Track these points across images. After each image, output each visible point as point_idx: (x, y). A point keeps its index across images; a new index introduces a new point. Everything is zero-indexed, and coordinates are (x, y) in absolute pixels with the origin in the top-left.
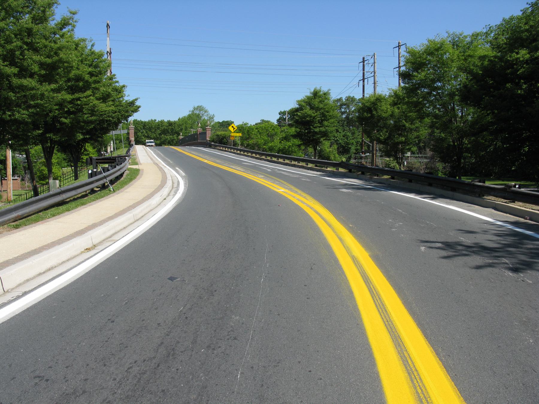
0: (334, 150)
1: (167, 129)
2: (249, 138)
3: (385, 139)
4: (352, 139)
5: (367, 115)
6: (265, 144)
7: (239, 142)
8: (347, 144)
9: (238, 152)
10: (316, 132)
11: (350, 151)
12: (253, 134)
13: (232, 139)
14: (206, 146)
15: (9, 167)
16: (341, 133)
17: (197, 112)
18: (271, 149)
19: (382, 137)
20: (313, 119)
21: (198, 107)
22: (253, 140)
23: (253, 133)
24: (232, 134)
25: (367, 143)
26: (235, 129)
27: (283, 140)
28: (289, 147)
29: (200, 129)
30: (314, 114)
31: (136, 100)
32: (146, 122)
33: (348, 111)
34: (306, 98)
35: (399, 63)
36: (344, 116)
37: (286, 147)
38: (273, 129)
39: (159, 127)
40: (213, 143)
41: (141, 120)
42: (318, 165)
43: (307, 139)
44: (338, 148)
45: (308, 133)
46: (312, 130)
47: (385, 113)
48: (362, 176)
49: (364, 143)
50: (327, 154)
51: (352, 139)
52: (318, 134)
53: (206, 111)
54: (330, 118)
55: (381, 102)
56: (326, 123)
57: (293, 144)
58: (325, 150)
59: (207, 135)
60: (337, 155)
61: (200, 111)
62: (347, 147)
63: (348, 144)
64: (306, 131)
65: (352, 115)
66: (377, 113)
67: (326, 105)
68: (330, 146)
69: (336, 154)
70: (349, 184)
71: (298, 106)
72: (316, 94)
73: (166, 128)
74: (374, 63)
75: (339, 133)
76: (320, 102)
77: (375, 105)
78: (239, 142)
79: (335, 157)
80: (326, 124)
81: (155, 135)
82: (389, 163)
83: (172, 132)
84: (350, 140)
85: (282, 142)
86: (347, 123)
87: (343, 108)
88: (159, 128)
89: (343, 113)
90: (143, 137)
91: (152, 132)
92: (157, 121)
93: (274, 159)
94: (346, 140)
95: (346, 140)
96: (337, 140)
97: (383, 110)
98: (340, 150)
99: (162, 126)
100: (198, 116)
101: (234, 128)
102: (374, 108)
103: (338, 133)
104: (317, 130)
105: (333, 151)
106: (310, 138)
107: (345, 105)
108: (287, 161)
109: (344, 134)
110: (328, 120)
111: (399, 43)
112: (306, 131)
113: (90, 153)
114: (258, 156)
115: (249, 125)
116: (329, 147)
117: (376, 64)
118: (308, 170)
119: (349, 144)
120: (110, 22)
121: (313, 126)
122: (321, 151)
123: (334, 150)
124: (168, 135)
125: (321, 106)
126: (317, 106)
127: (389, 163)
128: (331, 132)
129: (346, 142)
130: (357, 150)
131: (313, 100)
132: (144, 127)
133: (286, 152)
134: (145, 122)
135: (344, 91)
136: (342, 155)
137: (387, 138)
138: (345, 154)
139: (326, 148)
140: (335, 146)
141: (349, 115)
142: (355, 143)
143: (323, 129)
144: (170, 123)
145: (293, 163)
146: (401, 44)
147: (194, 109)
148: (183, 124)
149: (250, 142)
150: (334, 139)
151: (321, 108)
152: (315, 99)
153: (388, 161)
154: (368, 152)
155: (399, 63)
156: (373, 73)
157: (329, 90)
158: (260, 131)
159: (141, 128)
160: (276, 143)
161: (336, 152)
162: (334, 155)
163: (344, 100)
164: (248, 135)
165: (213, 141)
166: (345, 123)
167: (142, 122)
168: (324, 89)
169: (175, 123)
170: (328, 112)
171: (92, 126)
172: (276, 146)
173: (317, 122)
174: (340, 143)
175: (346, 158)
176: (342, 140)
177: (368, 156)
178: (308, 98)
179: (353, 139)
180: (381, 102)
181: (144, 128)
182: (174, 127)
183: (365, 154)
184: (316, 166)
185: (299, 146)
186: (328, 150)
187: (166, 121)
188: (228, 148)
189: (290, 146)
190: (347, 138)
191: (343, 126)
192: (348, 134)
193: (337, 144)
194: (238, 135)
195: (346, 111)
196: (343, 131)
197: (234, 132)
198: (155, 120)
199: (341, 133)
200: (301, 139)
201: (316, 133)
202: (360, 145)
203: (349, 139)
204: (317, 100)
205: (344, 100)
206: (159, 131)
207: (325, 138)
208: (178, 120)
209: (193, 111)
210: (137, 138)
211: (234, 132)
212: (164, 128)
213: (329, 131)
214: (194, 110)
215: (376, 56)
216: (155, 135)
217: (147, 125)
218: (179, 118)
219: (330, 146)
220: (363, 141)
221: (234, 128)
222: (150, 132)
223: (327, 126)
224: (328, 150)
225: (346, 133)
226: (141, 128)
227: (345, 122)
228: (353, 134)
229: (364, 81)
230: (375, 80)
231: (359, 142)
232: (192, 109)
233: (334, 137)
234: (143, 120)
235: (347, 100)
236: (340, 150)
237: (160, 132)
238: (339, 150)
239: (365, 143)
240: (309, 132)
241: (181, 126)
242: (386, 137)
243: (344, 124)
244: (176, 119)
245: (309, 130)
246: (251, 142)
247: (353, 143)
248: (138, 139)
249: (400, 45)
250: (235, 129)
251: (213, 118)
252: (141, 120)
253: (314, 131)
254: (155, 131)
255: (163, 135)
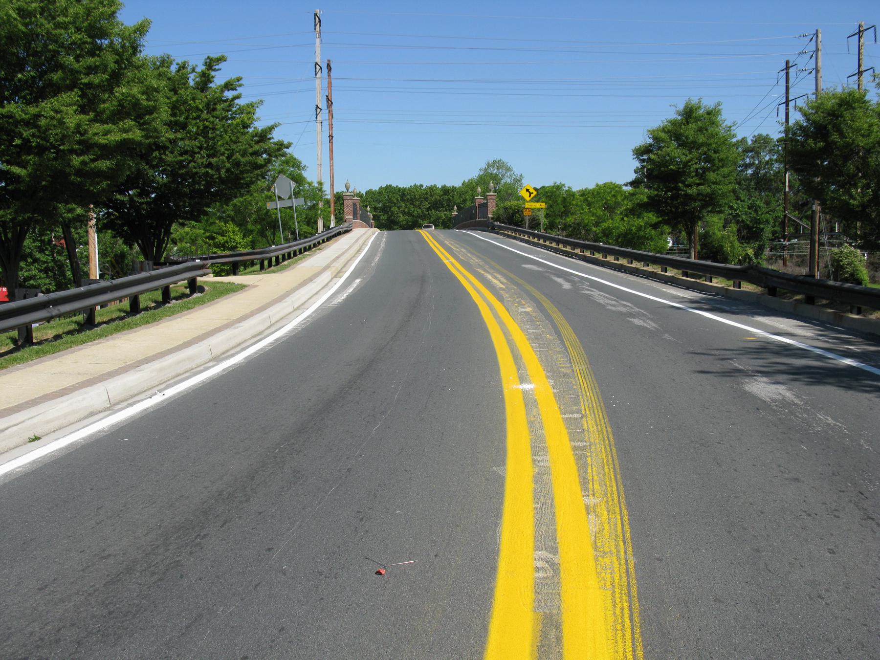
0: (732, 235)
1: (440, 200)
2: (566, 213)
3: (864, 206)
4: (766, 213)
5: (815, 144)
6: (597, 224)
7: (544, 221)
8: (756, 223)
9: (536, 240)
10: (691, 195)
11: (762, 235)
12: (573, 205)
13: (526, 214)
14: (486, 229)
15: (94, 274)
16: (744, 201)
17: (493, 171)
18: (607, 233)
19: (855, 199)
20: (683, 168)
21: (494, 162)
22: (575, 217)
23: (574, 202)
24: (527, 205)
25: (794, 221)
26: (532, 196)
27: (627, 216)
28: (640, 228)
29: (479, 197)
30: (686, 156)
31: (271, 129)
32: (405, 189)
33: (757, 162)
34: (669, 124)
35: (859, 66)
36: (750, 172)
37: (633, 228)
38: (614, 196)
39: (427, 198)
40: (497, 223)
41: (397, 186)
42: (690, 272)
43: (671, 212)
44: (739, 230)
45: (673, 198)
46: (682, 190)
47: (863, 136)
48: (807, 309)
49: (788, 220)
50: (717, 242)
51: (766, 213)
52: (695, 200)
53: (508, 169)
54: (720, 164)
55: (854, 108)
56: (711, 176)
57: (646, 223)
58: (714, 233)
59: (489, 208)
60: (737, 244)
61: (498, 169)
62: (756, 227)
63: (757, 221)
64: (669, 194)
65: (764, 169)
66: (842, 135)
67: (712, 136)
68: (724, 227)
69: (736, 240)
70: (773, 343)
71: (651, 141)
72: (689, 114)
73: (438, 198)
74: (817, 50)
75: (741, 201)
76: (700, 130)
77: (837, 119)
78: (544, 221)
79: (732, 247)
80: (713, 179)
81: (420, 211)
82: (840, 257)
83: (448, 205)
84: (762, 214)
85: (625, 219)
86: (757, 184)
87: (747, 157)
88: (426, 199)
89: (747, 166)
90: (401, 215)
91: (415, 206)
92: (424, 187)
93: (599, 256)
94: (754, 215)
95: (754, 215)
96: (738, 215)
97: (858, 130)
98: (743, 234)
99: (432, 196)
100: (496, 178)
101: (530, 194)
102: (833, 127)
103: (739, 202)
104: (692, 191)
105: (729, 236)
106: (677, 208)
107: (751, 151)
108: (623, 262)
109: (751, 204)
110: (718, 169)
111: (860, 26)
112: (669, 194)
113: (238, 245)
114: (568, 249)
115: (567, 189)
116: (722, 228)
117: (820, 53)
118: (666, 283)
119: (760, 223)
120: (320, 12)
121: (683, 182)
122: (705, 236)
123: (732, 235)
124: (441, 211)
125: (701, 139)
126: (691, 139)
127: (840, 257)
128: (724, 195)
129: (755, 218)
130: (774, 233)
131: (683, 127)
132: (402, 197)
133: (634, 238)
134: (404, 190)
135: (749, 117)
136: (747, 243)
137: (869, 201)
138: (751, 241)
139: (716, 231)
140: (734, 227)
141: (758, 168)
142: (772, 221)
143: (705, 189)
144: (446, 191)
145: (635, 265)
146: (864, 28)
147: (488, 165)
148: (467, 192)
149: (568, 220)
150: (732, 213)
151: (702, 145)
152: (688, 124)
153: (837, 254)
154: (795, 238)
155: (859, 66)
156: (814, 72)
157: (719, 104)
158: (589, 199)
159: (397, 200)
160: (618, 223)
161: (734, 238)
162: (731, 243)
163: (750, 142)
164: (564, 207)
165: (498, 219)
166: (752, 183)
167: (399, 189)
168: (708, 103)
169: (454, 189)
170: (716, 152)
171: (104, 184)
172: (618, 228)
173: (693, 174)
174: (743, 221)
175: (753, 248)
176: (746, 214)
177: (796, 244)
178: (674, 123)
179: (768, 212)
180: (854, 108)
181: (403, 200)
182: (452, 197)
183: (789, 241)
184: (685, 274)
185: (655, 226)
186: (719, 234)
187: (440, 187)
188: (520, 232)
189: (641, 226)
190: (756, 211)
191: (748, 189)
192: (758, 203)
193: (737, 222)
194: (538, 205)
195: (754, 164)
196: (749, 199)
197: (531, 201)
198: (421, 186)
199: (744, 201)
200: (659, 212)
201: (689, 198)
202: (780, 224)
203: (760, 213)
204: (693, 126)
205: (750, 142)
206: (427, 204)
207: (710, 209)
208: (463, 184)
209: (486, 170)
210: (391, 216)
211: (531, 201)
212: (436, 199)
213: (720, 192)
214: (488, 167)
215: (820, 35)
216: (420, 211)
217: (408, 194)
218: (464, 182)
219: (724, 227)
220: (785, 216)
221: (530, 194)
222: (412, 206)
223: (714, 183)
224: (719, 234)
225: (753, 201)
226: (397, 200)
227: (751, 182)
228: (767, 203)
229: (787, 105)
230: (819, 87)
231: (779, 217)
232: (484, 166)
233: (731, 208)
234: (401, 186)
235: (756, 141)
236: (743, 234)
237: (428, 206)
238: (741, 233)
239: (790, 219)
240: (675, 197)
241: (463, 194)
242: (866, 199)
243: (750, 185)
244: (458, 184)
245: (674, 192)
246: (570, 220)
247: (767, 221)
248: (393, 218)
249: (861, 29)
250: (532, 196)
251: (520, 181)
252: (397, 186)
253: (686, 195)
254: (420, 204)
255: (433, 211)
